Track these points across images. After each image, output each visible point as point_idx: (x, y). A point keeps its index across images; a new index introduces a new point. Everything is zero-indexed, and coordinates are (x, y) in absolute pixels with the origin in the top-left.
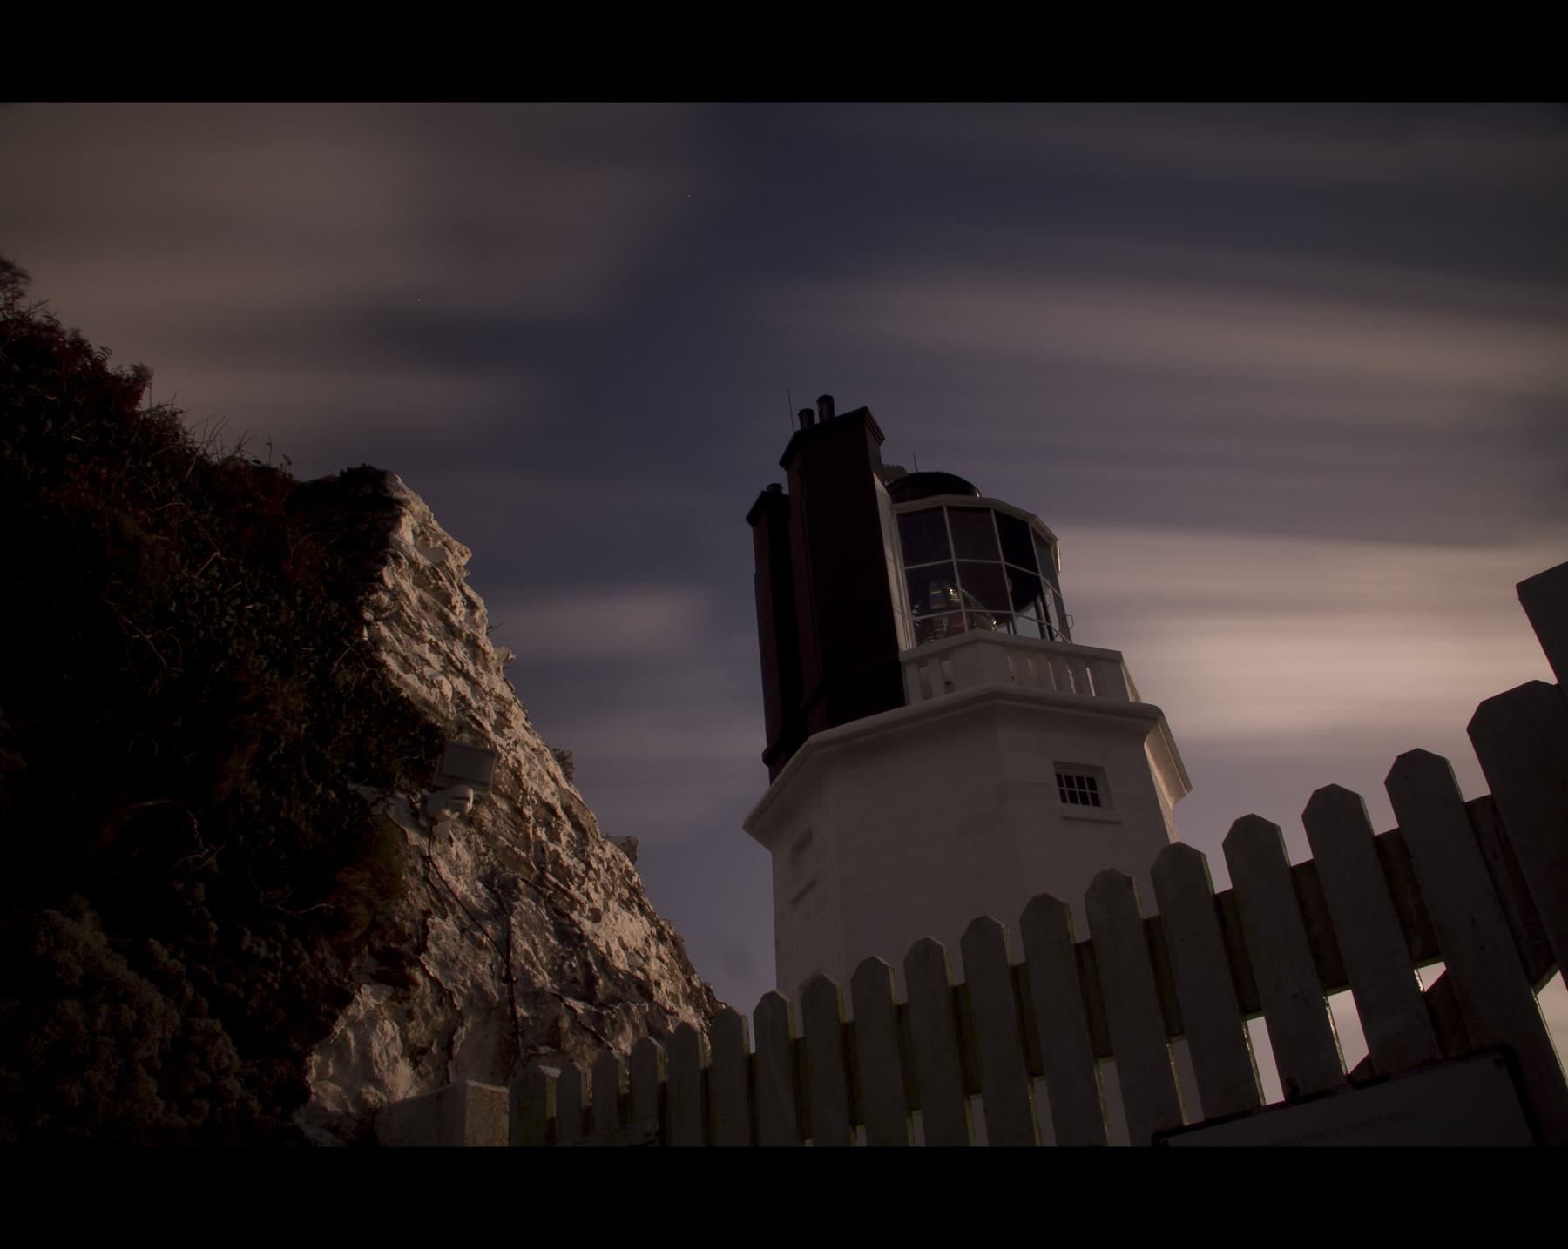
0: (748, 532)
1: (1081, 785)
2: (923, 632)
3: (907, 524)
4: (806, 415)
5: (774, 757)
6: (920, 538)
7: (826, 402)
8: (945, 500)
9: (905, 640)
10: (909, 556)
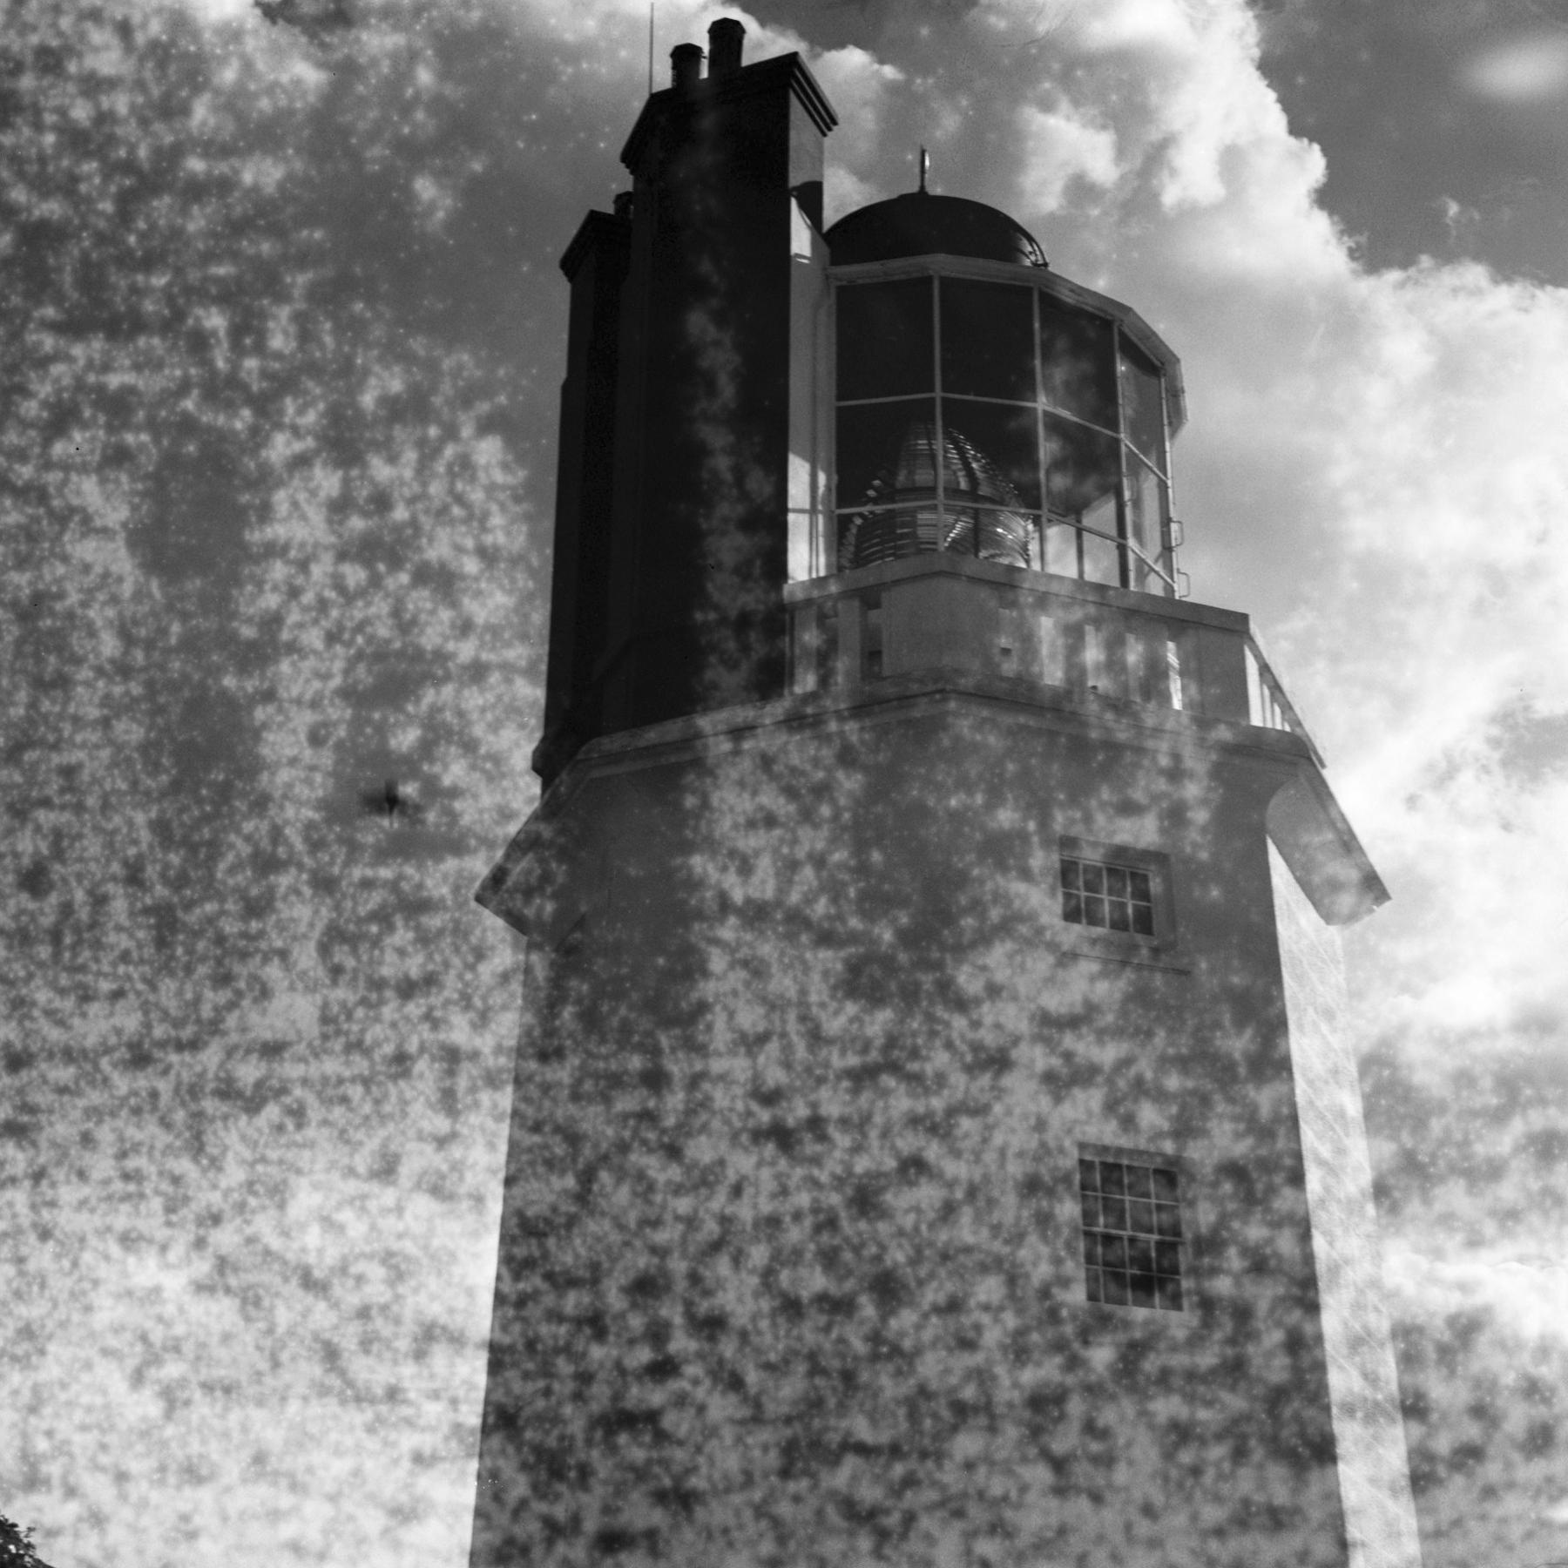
0: (560, 292)
2: (852, 541)
3: (851, 308)
4: (684, 56)
8: (942, 264)
9: (804, 559)
10: (852, 371)
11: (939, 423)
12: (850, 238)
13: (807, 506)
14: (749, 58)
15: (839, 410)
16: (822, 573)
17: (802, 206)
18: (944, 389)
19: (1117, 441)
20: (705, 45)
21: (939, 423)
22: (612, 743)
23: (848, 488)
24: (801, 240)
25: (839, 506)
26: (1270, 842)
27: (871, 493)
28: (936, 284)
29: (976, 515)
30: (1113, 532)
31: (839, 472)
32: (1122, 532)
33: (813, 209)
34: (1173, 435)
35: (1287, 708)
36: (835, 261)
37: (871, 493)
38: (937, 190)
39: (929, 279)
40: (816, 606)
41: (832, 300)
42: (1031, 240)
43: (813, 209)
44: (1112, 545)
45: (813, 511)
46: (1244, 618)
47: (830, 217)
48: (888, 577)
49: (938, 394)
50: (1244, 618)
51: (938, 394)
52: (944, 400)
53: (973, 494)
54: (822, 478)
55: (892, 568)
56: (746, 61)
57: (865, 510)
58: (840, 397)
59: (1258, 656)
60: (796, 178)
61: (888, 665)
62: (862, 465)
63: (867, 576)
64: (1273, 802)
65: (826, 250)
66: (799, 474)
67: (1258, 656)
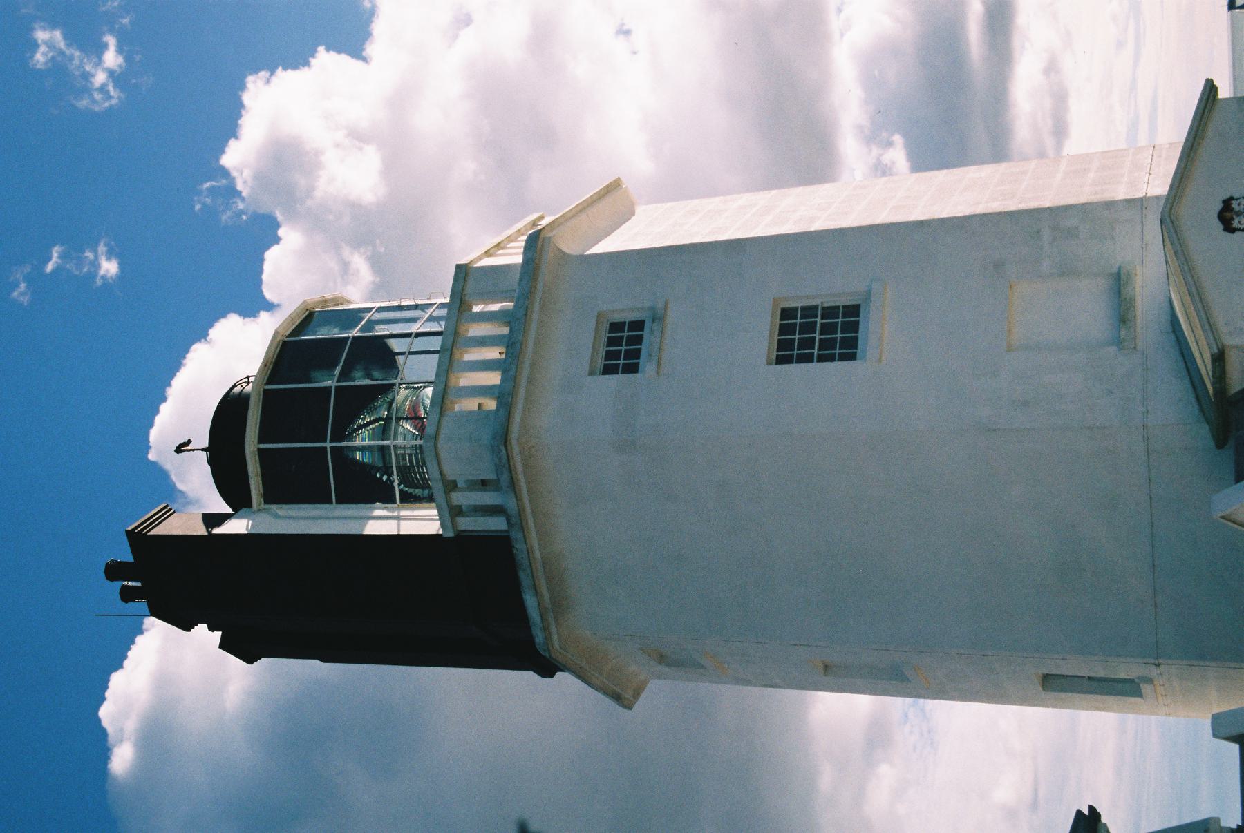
1: (629, 355)
2: (415, 492)
3: (277, 494)
4: (127, 595)
5: (547, 668)
6: (290, 483)
7: (114, 571)
8: (251, 444)
9: (422, 521)
10: (316, 495)
11: (344, 444)
12: (237, 496)
13: (396, 522)
14: (128, 557)
15: (339, 501)
16: (436, 512)
17: (219, 524)
18: (325, 441)
19: (354, 338)
20: (118, 585)
21: (344, 444)
22: (539, 638)
23: (386, 497)
24: (237, 526)
25: (260, 442)
26: (588, 253)
27: (385, 478)
28: (262, 446)
29: (398, 419)
30: (408, 340)
31: (373, 502)
32: (408, 335)
33: (219, 519)
34: (349, 302)
35: (510, 239)
36: (249, 505)
37: (385, 478)
38: (206, 444)
39: (259, 449)
40: (452, 513)
41: (273, 507)
42: (235, 386)
43: (219, 519)
44: (416, 340)
45: (398, 518)
46: (458, 267)
47: (226, 509)
48: (438, 476)
49: (328, 445)
50: (458, 267)
51: (328, 445)
52: (332, 441)
53: (388, 420)
54: (377, 513)
55: (432, 472)
56: (131, 559)
57: (396, 484)
58: (331, 502)
59: (480, 258)
60: (201, 530)
61: (490, 475)
62: (367, 486)
63: (437, 488)
64: (565, 250)
65: (243, 510)
66: (374, 528)
67: (480, 258)
